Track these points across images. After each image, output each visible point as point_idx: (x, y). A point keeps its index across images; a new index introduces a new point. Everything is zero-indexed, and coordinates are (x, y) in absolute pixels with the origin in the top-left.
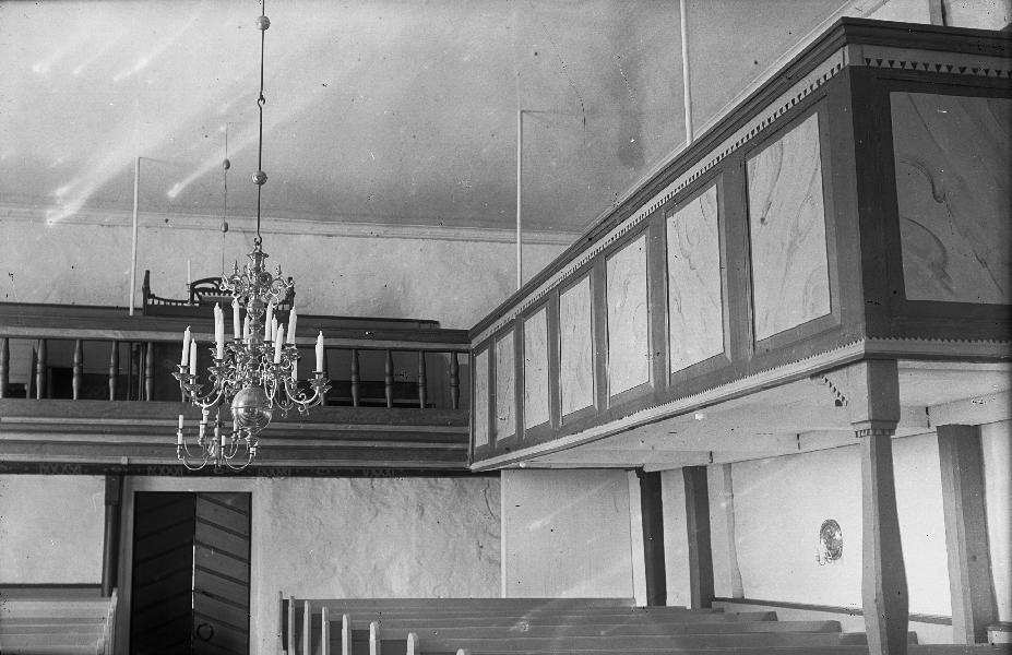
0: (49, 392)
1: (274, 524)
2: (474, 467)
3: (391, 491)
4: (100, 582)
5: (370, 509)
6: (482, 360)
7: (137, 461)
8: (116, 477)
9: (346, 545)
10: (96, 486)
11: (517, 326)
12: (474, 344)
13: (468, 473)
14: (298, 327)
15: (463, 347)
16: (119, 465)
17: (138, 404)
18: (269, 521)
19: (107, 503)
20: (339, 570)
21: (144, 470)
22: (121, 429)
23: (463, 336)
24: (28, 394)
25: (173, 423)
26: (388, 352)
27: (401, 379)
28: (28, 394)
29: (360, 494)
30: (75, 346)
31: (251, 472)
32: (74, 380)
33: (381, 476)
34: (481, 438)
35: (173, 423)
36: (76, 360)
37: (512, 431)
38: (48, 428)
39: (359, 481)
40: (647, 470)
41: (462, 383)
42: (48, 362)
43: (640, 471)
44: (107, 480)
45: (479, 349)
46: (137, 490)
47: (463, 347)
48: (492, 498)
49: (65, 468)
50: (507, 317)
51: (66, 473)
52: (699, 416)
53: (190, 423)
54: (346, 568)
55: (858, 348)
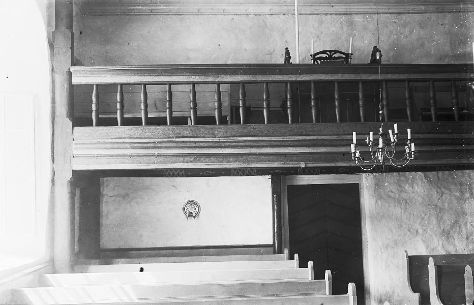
0: (234, 122)
1: (376, 202)
3: (450, 180)
4: (271, 243)
5: (438, 192)
8: (279, 177)
9: (423, 215)
10: (264, 184)
16: (300, 167)
17: (308, 125)
18: (373, 201)
19: (273, 193)
20: (420, 231)
21: (297, 171)
22: (278, 143)
24: (229, 123)
25: (349, 137)
26: (431, 82)
27: (273, 109)
28: (229, 123)
29: (430, 182)
30: (334, 86)
31: (357, 170)
33: (443, 170)
35: (349, 137)
36: (265, 97)
38: (251, 144)
42: (200, 105)
44: (272, 179)
46: (288, 184)
49: (247, 172)
51: (247, 175)
53: (361, 137)
54: (425, 230)
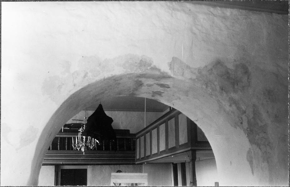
2: (136, 163)
6: (138, 140)
7: (64, 163)
8: (57, 167)
11: (150, 131)
12: (137, 136)
13: (135, 164)
14: (63, 138)
15: (134, 137)
23: (135, 135)
32: (58, 146)
34: (138, 157)
37: (143, 156)
39: (111, 166)
40: (174, 163)
41: (134, 144)
43: (173, 163)
45: (138, 138)
47: (134, 137)
48: (142, 166)
50: (146, 131)
52: (172, 156)
55: (190, 148)
